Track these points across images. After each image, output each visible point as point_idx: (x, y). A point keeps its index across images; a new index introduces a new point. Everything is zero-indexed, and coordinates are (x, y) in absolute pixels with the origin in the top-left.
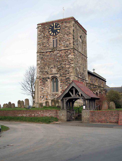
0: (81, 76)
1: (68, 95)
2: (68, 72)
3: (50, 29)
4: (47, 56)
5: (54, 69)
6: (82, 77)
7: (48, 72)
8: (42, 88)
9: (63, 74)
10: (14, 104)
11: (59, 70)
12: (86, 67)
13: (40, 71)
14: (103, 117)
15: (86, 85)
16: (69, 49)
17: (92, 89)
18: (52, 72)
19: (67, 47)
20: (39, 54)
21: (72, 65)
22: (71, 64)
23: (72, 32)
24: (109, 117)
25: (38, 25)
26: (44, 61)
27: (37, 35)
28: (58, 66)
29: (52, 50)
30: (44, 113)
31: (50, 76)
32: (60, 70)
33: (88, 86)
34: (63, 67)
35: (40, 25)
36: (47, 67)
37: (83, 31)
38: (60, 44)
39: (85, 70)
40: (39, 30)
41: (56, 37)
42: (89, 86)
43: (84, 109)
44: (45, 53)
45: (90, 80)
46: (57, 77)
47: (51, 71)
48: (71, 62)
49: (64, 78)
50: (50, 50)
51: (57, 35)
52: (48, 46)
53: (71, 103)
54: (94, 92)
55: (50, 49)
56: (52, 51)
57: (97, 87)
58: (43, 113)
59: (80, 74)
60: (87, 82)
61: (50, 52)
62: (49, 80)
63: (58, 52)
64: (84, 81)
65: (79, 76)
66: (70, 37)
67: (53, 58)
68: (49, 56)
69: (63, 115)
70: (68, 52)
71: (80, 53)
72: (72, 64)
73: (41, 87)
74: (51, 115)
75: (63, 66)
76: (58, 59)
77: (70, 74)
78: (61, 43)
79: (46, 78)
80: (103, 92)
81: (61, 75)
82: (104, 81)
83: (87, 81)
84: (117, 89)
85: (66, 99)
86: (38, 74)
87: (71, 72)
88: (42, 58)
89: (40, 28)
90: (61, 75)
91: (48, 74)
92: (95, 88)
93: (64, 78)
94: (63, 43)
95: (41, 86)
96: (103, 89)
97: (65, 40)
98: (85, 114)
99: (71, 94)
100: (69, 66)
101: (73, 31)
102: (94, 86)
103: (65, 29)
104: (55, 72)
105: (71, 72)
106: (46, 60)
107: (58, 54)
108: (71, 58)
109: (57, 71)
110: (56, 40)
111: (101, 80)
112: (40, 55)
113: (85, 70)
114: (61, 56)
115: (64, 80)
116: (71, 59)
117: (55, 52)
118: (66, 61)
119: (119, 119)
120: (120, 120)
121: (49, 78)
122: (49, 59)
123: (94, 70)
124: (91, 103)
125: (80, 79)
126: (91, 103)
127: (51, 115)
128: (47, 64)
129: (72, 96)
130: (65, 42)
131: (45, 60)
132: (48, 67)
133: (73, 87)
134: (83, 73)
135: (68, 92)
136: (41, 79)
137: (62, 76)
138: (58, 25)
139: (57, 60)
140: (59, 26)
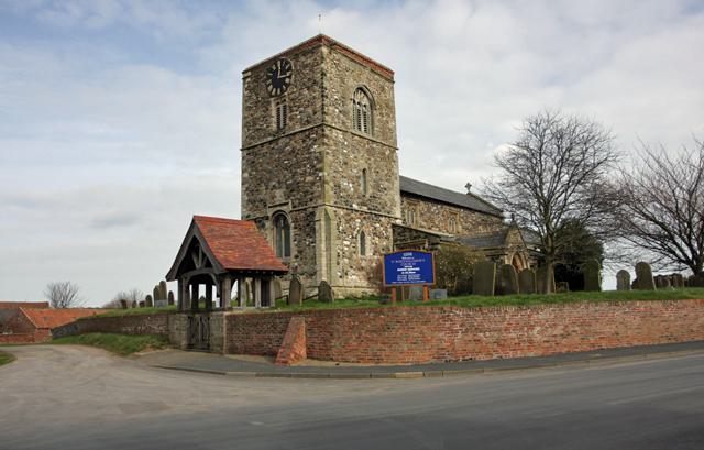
3: (269, 78)
11: (291, 190)
13: (249, 201)
14: (254, 334)
15: (390, 230)
19: (308, 122)
25: (243, 73)
31: (270, 213)
32: (292, 191)
35: (249, 73)
43: (217, 310)
48: (318, 166)
50: (270, 139)
55: (270, 135)
60: (399, 222)
61: (270, 142)
64: (383, 219)
65: (355, 206)
89: (249, 80)
92: (415, 238)
116: (317, 158)
121: (267, 218)
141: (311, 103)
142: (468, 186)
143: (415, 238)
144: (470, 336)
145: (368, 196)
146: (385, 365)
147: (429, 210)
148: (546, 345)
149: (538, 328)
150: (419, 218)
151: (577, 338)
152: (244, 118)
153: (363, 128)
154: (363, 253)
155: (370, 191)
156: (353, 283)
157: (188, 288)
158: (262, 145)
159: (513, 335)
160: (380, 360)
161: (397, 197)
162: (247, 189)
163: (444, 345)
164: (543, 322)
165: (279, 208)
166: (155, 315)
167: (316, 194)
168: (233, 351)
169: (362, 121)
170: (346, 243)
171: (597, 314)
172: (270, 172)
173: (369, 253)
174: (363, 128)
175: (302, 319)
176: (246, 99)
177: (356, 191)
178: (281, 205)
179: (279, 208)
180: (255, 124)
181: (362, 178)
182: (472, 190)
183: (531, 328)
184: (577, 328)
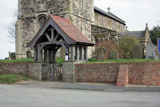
1: (43, 39)
5: (42, 4)
6: (84, 17)
7: (34, 10)
8: (26, 32)
9: (54, 12)
11: (49, 5)
13: (23, 8)
14: (94, 73)
15: (91, 28)
30: (10, 68)
31: (36, 15)
32: (50, 5)
33: (93, 29)
39: (89, 6)
42: (95, 30)
43: (67, 61)
45: (99, 21)
53: (52, 51)
54: (103, 37)
57: (106, 31)
58: (9, 68)
60: (93, 24)
62: (35, 21)
64: (88, 22)
65: (79, 15)
69: (36, 71)
73: (24, 31)
74: (19, 70)
77: (65, 11)
79: (31, 17)
82: (123, 23)
83: (93, 22)
84: (136, 34)
85: (41, 46)
86: (20, 13)
87: (65, 9)
92: (103, 32)
95: (24, 30)
98: (68, 68)
99: (48, 36)
102: (103, 30)
104: (43, 8)
111: (117, 23)
113: (89, 6)
119: (119, 77)
120: (119, 79)
121: (35, 18)
123: (109, 9)
124: (78, 51)
126: (78, 51)
127: (19, 70)
129: (50, 40)
132: (33, 2)
133: (50, 26)
134: (86, 11)
135: (44, 33)
136: (24, 20)
142: (109, 9)
143: (103, 32)
145: (84, 10)
147: (102, 19)
155: (84, 8)
156: (48, 51)
157: (42, 51)
165: (42, 13)
166: (124, 63)
168: (79, 80)
175: (127, 66)
177: (80, 8)
179: (42, 13)
182: (110, 11)
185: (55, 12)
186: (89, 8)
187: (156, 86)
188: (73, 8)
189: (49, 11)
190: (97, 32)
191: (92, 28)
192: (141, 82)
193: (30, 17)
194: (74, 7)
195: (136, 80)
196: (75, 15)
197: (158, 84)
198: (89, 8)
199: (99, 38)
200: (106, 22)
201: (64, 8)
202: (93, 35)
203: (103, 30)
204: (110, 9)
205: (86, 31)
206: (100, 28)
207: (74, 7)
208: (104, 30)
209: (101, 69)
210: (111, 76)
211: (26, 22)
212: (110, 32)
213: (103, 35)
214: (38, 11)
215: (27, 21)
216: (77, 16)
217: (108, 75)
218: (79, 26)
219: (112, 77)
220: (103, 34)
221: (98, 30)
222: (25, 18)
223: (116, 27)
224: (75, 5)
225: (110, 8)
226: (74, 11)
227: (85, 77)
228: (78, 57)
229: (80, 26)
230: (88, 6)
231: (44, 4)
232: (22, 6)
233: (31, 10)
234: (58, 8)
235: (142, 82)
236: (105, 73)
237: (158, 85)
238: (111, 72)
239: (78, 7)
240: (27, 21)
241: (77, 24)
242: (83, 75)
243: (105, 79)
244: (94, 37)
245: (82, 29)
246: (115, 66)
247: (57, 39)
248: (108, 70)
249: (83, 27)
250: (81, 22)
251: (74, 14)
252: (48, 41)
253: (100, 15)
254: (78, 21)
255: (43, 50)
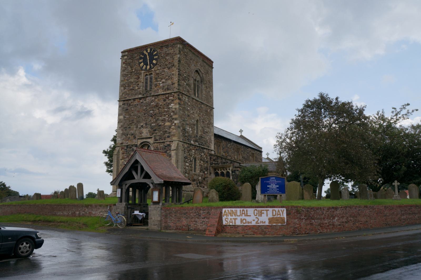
0: (196, 141)
2: (168, 134)
3: (141, 58)
4: (135, 107)
6: (199, 144)
7: (136, 136)
10: (101, 193)
11: (153, 131)
12: (211, 124)
14: (183, 219)
15: (208, 157)
16: (171, 93)
17: (220, 165)
18: (143, 134)
19: (168, 89)
20: (122, 103)
21: (176, 122)
22: (173, 119)
23: (176, 63)
24: (193, 220)
25: (122, 52)
26: (130, 115)
27: (121, 70)
28: (153, 123)
29: (143, 95)
31: (140, 142)
32: (155, 130)
33: (212, 159)
34: (160, 126)
35: (127, 53)
36: (133, 127)
37: (203, 61)
38: (156, 85)
39: (207, 129)
40: (124, 61)
41: (150, 72)
42: (214, 160)
44: (132, 101)
46: (149, 143)
47: (141, 134)
48: (174, 117)
49: (161, 145)
50: (140, 96)
51: (153, 69)
52: (137, 88)
54: (224, 170)
55: (140, 94)
56: (144, 97)
58: (91, 210)
59: (194, 139)
60: (213, 152)
61: (140, 99)
63: (153, 98)
64: (205, 150)
65: (192, 142)
66: (173, 73)
67: (144, 110)
68: (139, 106)
70: (170, 98)
71: (194, 100)
72: (176, 119)
75: (161, 123)
76: (153, 111)
78: (159, 82)
79: (132, 145)
80: (238, 170)
81: (157, 140)
85: (126, 185)
87: (173, 135)
88: (127, 110)
89: (126, 57)
90: (157, 140)
91: (135, 138)
92: (224, 163)
93: (162, 145)
94: (161, 82)
95: (123, 160)
96: (238, 165)
97: (164, 78)
99: (134, 173)
100: (170, 124)
101: (179, 61)
102: (224, 161)
103: (166, 59)
104: (146, 134)
105: (174, 135)
106: (133, 113)
107: (153, 103)
108: (174, 110)
109: (150, 132)
110: (151, 78)
112: (123, 105)
114: (157, 106)
115: (161, 149)
116: (173, 112)
117: (148, 99)
118: (165, 115)
122: (138, 111)
123: (241, 131)
125: (195, 147)
128: (135, 121)
129: (136, 176)
130: (164, 80)
131: (132, 114)
132: (135, 126)
134: (202, 137)
137: (157, 142)
138: (154, 51)
139: (151, 113)
140: (156, 52)
141: (170, 78)
142: (241, 131)
144: (308, 222)
145: (198, 136)
146: (268, 236)
147: (226, 146)
148: (339, 227)
149: (336, 218)
150: (221, 151)
151: (352, 223)
152: (121, 81)
153: (197, 95)
154: (195, 171)
158: (134, 99)
159: (326, 221)
160: (266, 233)
161: (213, 138)
162: (122, 126)
163: (297, 226)
164: (339, 215)
165: (145, 140)
167: (172, 134)
169: (196, 90)
170: (187, 164)
171: (360, 212)
172: (139, 117)
173: (198, 171)
174: (197, 95)
176: (123, 70)
177: (193, 132)
178: (146, 138)
179: (145, 140)
180: (129, 86)
181: (196, 126)
183: (334, 218)
184: (352, 219)
185: (161, 139)
186: (207, 133)
187: (253, 236)
188: (183, 134)
189: (153, 138)
190: (217, 163)
191: (211, 158)
192: (235, 231)
193: (131, 144)
194: (184, 133)
195: (229, 228)
196: (186, 142)
197: (255, 233)
198: (207, 133)
199: (220, 170)
200: (233, 149)
201: (172, 134)
202: (212, 167)
203: (224, 161)
204: (242, 131)
205: (202, 162)
206: (221, 158)
207: (184, 133)
208: (225, 160)
209: (191, 214)
210: (203, 223)
211: (126, 150)
212: (232, 163)
213: (224, 167)
214: (141, 138)
215: (127, 150)
216: (189, 144)
217: (199, 221)
218: (191, 156)
219: (203, 224)
220: (224, 166)
221: (218, 160)
222: (125, 146)
223: (247, 155)
224: (186, 130)
225: (242, 130)
226: (184, 137)
227: (174, 224)
228: (143, 201)
229: (193, 156)
230: (205, 131)
231: (148, 129)
232: (122, 131)
233: (133, 136)
234: (164, 134)
235: (237, 231)
236: (195, 219)
237: (255, 234)
238: (202, 219)
239: (191, 132)
240: (128, 149)
241: (188, 153)
242: (171, 221)
243: (196, 227)
244: (213, 169)
245: (197, 159)
246: (207, 211)
247: (144, 176)
248: (199, 216)
249: (198, 157)
250: (195, 151)
251: (185, 141)
252: (134, 178)
253: (223, 141)
254: (190, 149)
255: (131, 189)
